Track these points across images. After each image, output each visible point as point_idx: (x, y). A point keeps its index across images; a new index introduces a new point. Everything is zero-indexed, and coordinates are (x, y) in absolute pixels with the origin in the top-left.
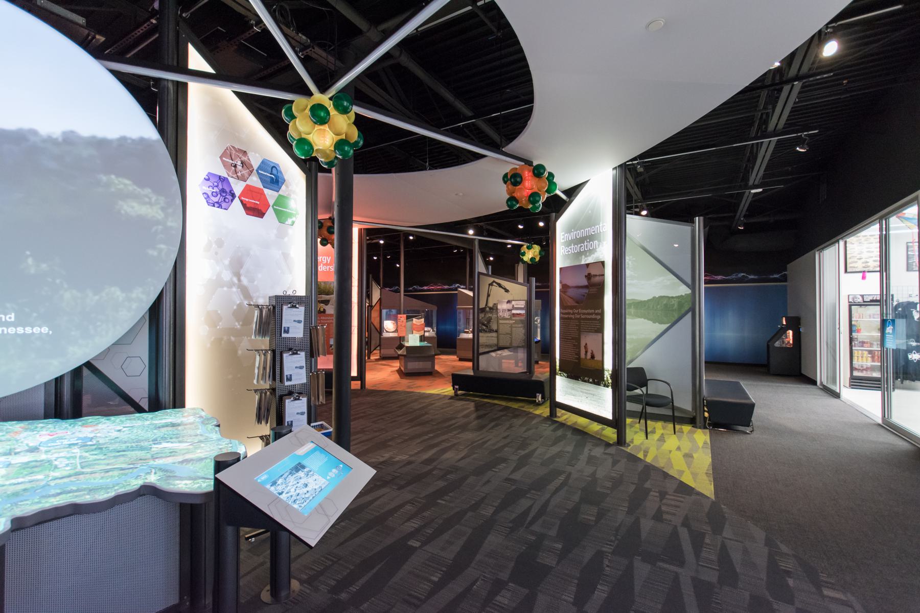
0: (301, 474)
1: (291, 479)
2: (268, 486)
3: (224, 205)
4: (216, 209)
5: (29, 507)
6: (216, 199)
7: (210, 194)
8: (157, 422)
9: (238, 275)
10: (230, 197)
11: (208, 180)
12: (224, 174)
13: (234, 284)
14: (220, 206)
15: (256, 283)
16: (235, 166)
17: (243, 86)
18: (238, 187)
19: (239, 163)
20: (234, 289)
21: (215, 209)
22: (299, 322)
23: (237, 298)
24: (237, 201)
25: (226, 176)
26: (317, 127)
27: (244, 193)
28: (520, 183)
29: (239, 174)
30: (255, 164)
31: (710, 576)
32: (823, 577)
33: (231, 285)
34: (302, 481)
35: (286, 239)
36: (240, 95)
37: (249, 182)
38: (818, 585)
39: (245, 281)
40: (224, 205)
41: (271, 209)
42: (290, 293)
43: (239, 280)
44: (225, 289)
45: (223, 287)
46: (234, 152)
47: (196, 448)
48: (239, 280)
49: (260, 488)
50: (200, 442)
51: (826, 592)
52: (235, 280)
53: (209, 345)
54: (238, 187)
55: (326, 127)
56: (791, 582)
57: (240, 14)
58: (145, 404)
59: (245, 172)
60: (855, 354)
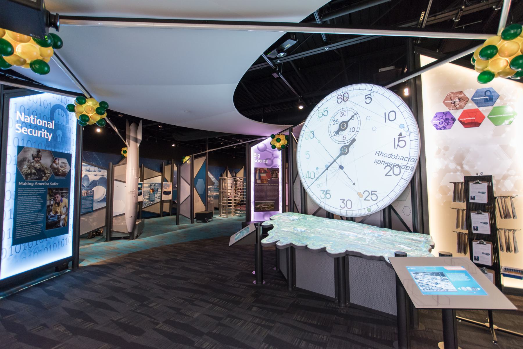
0: (439, 278)
1: (429, 277)
2: (411, 273)
3: (447, 127)
4: (443, 131)
5: (351, 249)
6: (441, 126)
7: (438, 124)
8: (407, 237)
9: (461, 165)
10: (452, 122)
11: (437, 116)
12: (446, 110)
13: (458, 170)
14: (445, 128)
15: (476, 168)
16: (454, 103)
17: (464, 53)
18: (457, 114)
19: (457, 100)
20: (458, 173)
21: (442, 131)
22: (483, 193)
24: (457, 122)
25: (448, 110)
26: (490, 61)
28: (446, 99)
29: (458, 106)
33: (456, 171)
34: (436, 281)
35: (503, 136)
36: (454, 62)
37: (465, 108)
40: (447, 127)
42: (479, 174)
43: (462, 167)
44: (452, 173)
45: (450, 172)
46: (452, 95)
47: (411, 251)
48: (462, 167)
49: (407, 273)
50: (416, 249)
52: (459, 168)
53: (442, 204)
54: (457, 114)
55: (498, 56)
57: (444, 21)
58: (411, 229)
59: (462, 104)
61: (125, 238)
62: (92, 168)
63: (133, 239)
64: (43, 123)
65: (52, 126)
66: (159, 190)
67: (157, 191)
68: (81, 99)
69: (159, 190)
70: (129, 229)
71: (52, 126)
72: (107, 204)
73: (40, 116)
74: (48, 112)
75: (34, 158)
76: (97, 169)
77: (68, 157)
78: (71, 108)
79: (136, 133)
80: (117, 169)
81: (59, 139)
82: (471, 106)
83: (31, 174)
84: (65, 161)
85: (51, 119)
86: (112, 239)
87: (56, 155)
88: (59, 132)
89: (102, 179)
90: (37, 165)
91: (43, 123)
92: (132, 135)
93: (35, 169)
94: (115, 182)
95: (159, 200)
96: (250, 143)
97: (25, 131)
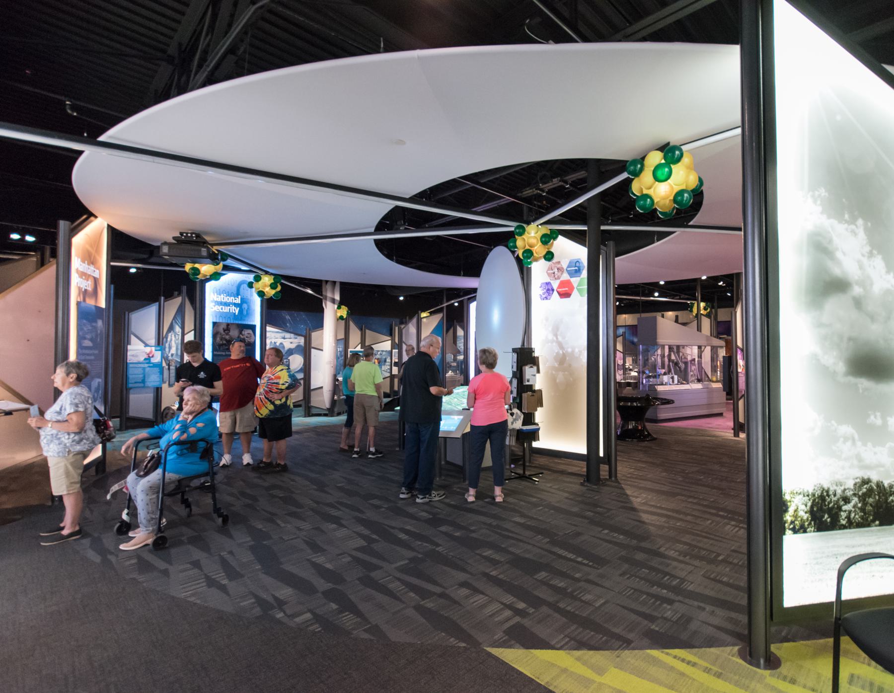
12: (548, 280)
14: (546, 298)
18: (555, 284)
19: (556, 270)
23: (556, 349)
24: (555, 293)
27: (559, 287)
30: (565, 265)
31: (376, 575)
32: (317, 628)
33: (552, 341)
37: (562, 279)
38: (317, 618)
39: (560, 339)
41: (575, 290)
51: (308, 616)
54: (555, 284)
56: (334, 606)
60: (744, 542)
61: (326, 415)
62: (288, 335)
63: (332, 416)
64: (231, 299)
65: (238, 301)
66: (388, 360)
67: (385, 361)
68: (258, 279)
69: (388, 360)
70: (327, 404)
71: (238, 301)
72: (305, 376)
73: (229, 294)
74: (234, 289)
75: (224, 330)
76: (292, 335)
77: (253, 328)
78: (250, 285)
79: (333, 293)
80: (314, 335)
81: (245, 313)
82: (565, 276)
83: (222, 345)
84: (250, 331)
85: (238, 294)
86: (309, 416)
87: (243, 327)
88: (245, 306)
89: (298, 346)
90: (227, 337)
91: (231, 299)
92: (329, 295)
93: (226, 340)
94: (313, 350)
95: (388, 375)
96: (469, 299)
97: (218, 308)
